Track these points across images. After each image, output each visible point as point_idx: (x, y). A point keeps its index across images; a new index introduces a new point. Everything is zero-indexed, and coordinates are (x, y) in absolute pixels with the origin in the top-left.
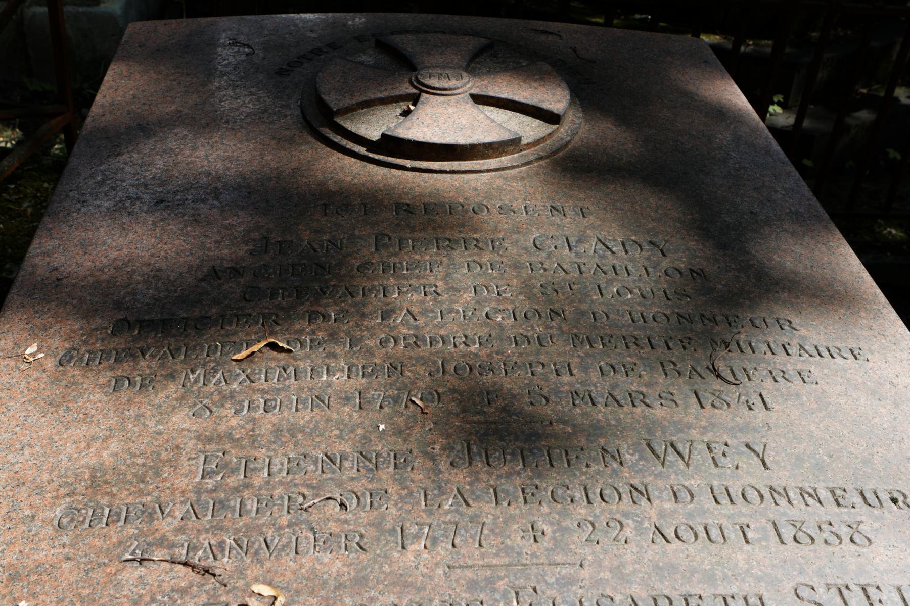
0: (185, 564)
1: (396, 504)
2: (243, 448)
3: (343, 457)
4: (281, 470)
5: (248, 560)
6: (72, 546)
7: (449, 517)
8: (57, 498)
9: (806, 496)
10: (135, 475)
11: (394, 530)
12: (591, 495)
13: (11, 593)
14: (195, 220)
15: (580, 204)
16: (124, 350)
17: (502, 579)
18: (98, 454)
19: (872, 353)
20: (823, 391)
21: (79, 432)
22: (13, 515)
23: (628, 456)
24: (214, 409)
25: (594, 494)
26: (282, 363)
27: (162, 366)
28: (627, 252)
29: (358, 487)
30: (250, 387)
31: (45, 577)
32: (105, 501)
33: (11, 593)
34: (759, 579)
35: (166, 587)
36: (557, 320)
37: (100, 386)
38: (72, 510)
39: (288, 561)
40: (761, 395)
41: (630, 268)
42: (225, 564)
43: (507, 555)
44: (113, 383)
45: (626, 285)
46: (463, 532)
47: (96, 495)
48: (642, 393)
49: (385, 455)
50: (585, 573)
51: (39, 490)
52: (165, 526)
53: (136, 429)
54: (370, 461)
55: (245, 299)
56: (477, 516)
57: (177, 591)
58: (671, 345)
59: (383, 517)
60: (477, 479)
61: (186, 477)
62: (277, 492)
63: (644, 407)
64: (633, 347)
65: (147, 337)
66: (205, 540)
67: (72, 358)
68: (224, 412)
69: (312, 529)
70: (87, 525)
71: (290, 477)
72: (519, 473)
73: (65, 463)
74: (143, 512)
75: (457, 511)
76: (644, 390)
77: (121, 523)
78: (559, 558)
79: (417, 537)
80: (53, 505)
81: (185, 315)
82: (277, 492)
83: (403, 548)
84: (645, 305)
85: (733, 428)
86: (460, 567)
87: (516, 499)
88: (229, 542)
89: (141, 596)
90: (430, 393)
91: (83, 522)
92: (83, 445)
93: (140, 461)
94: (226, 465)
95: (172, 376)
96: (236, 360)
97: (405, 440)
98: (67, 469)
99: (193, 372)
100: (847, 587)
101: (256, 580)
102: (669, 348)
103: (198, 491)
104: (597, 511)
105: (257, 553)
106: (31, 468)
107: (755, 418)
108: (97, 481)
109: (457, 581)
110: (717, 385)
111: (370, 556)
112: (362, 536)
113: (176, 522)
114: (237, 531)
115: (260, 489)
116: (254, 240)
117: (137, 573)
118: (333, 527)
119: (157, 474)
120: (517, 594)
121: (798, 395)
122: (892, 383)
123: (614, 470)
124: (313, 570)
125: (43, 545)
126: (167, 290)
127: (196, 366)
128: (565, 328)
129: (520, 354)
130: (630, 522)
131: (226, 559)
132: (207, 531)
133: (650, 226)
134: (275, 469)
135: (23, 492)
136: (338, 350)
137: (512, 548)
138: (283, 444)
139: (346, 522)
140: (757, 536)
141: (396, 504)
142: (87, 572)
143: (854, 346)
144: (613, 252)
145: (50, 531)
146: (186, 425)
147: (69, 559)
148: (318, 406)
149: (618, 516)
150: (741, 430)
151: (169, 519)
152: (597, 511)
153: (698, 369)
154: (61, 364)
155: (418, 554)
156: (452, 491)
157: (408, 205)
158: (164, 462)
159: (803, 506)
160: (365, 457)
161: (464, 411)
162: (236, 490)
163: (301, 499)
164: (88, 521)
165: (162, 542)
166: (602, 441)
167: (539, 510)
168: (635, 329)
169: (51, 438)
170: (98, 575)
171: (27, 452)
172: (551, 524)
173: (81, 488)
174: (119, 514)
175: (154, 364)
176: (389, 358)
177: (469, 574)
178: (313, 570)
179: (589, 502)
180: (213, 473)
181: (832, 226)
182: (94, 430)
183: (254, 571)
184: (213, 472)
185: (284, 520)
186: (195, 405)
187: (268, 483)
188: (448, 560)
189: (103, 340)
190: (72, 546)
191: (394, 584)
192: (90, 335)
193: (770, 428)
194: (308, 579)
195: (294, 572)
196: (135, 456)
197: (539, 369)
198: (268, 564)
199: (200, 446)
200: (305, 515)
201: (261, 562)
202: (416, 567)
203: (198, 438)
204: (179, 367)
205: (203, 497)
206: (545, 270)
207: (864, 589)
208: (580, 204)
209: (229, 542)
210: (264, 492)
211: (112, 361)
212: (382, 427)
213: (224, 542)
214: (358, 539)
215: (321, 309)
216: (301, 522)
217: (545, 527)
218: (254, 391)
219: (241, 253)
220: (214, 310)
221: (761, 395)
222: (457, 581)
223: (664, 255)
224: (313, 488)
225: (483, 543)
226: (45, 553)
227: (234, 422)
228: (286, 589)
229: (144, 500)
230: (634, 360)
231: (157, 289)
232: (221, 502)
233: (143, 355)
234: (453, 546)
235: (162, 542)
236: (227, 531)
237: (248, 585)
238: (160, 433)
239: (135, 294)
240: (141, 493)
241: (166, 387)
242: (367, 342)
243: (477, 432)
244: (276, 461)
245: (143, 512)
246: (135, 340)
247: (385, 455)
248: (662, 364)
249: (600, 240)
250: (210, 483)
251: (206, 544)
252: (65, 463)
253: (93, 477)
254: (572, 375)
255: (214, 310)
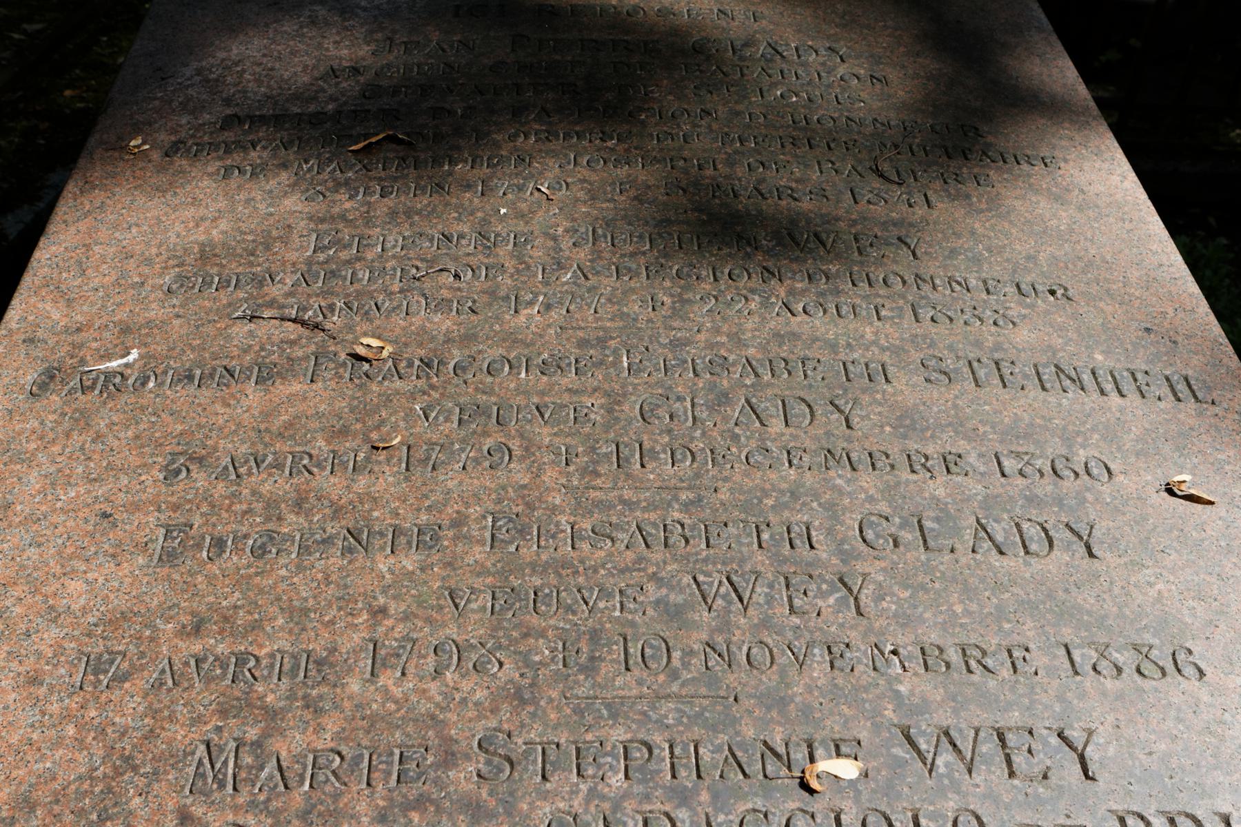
0: (294, 321)
1: (512, 276)
2: (356, 227)
3: (461, 236)
4: (394, 246)
5: (358, 319)
6: (181, 306)
7: (566, 287)
8: (166, 268)
9: (954, 284)
10: (245, 250)
11: (508, 297)
12: (718, 274)
13: (123, 343)
14: (313, 22)
15: (753, 8)
16: (233, 143)
17: (614, 339)
18: (207, 232)
19: (1066, 161)
20: (999, 193)
21: (190, 213)
22: (123, 282)
23: (764, 242)
24: (328, 194)
25: (722, 273)
26: (401, 154)
27: (274, 156)
28: (799, 57)
29: (473, 261)
30: (366, 176)
31: (156, 331)
32: (215, 270)
33: (123, 343)
34: (883, 349)
35: (275, 339)
36: (708, 119)
37: (210, 175)
38: (180, 278)
39: (399, 321)
40: (925, 195)
41: (800, 72)
42: (335, 322)
43: (621, 319)
44: (222, 171)
45: (793, 88)
46: (578, 300)
47: (205, 265)
48: (792, 189)
49: (504, 235)
50: (702, 337)
51: (149, 262)
52: (275, 291)
53: (246, 211)
54: (488, 240)
55: (364, 96)
56: (594, 288)
57: (286, 343)
58: (832, 145)
59: (498, 287)
60: (600, 258)
61: (300, 249)
62: (389, 265)
63: (790, 200)
64: (789, 147)
65: (257, 132)
66: (315, 303)
67: (178, 149)
68: (338, 197)
69: (424, 295)
70: (196, 290)
71: (404, 252)
72: (644, 253)
73: (173, 239)
74: (253, 280)
75: (575, 283)
76: (794, 185)
77: (231, 289)
78: (676, 324)
79: (531, 303)
80: (161, 275)
81: (299, 111)
82: (389, 265)
83: (516, 312)
84: (810, 108)
85: (885, 222)
86: (573, 328)
87: (638, 274)
88: (339, 304)
89: (250, 346)
90: (558, 183)
91: (193, 287)
92: (191, 225)
93: (250, 238)
94: (339, 241)
95: (284, 166)
96: (352, 151)
97: (527, 223)
98: (175, 245)
99: (306, 162)
100: (979, 361)
101: (365, 334)
102: (830, 148)
103: (309, 262)
104: (723, 288)
105: (367, 313)
106: (138, 244)
107: (914, 214)
108: (206, 254)
109: (568, 339)
110: (877, 183)
111: (480, 317)
112: (474, 302)
113: (286, 288)
114: (348, 295)
115: (373, 261)
116: (377, 41)
117: (246, 328)
118: (445, 293)
119: (268, 248)
120: (628, 351)
121: (968, 197)
122: (1082, 191)
123: (747, 253)
124: (423, 328)
125: (154, 306)
126: (280, 88)
127: (311, 156)
128: (715, 126)
129: (661, 150)
130: (756, 297)
131: (335, 318)
132: (318, 295)
133: (832, 32)
134: (388, 245)
135: (132, 264)
136: (462, 143)
137: (628, 315)
138: (398, 224)
139: (459, 289)
140: (890, 314)
141: (512, 276)
142: (197, 327)
143: (1047, 154)
144: (783, 57)
145: (160, 294)
146: (299, 208)
147: (178, 316)
148: (437, 192)
149: (744, 292)
150: (895, 225)
151: (280, 286)
152: (723, 288)
153: (859, 169)
154: (167, 155)
155: (530, 317)
156: (571, 266)
157: (552, 6)
158: (275, 239)
159: (948, 292)
160: (484, 237)
161: (593, 199)
162: (348, 262)
163: (414, 271)
164: (197, 287)
165: (272, 304)
166: (739, 228)
167: (661, 284)
168: (794, 129)
169: (158, 218)
170: (209, 329)
171: (134, 230)
172: (672, 296)
173: (190, 260)
174: (229, 282)
175: (265, 155)
176: (516, 150)
177: (580, 334)
178: (423, 328)
179: (716, 280)
180: (325, 248)
181: (1054, 38)
182: (202, 211)
183: (366, 327)
184: (325, 247)
185: (396, 287)
186: (307, 190)
187: (381, 257)
188: (562, 322)
189: (211, 133)
190: (181, 306)
191: (504, 340)
192: (197, 130)
193: (928, 224)
194: (418, 334)
195: (404, 329)
196: (245, 233)
197: (681, 163)
198: (377, 322)
199: (312, 226)
200: (417, 283)
201: (371, 321)
202: (527, 328)
203: (311, 219)
204: (291, 158)
205: (314, 268)
206: (701, 71)
207: (997, 363)
208: (753, 8)
209: (339, 304)
210: (376, 264)
211: (221, 152)
212: (503, 211)
213: (334, 304)
214: (470, 304)
215: (447, 106)
216: (413, 289)
217: (665, 299)
218: (370, 179)
219: (361, 53)
220: (330, 107)
221: (925, 195)
222: (568, 339)
223: (842, 60)
224: (427, 261)
225: (599, 310)
226: (155, 312)
227: (348, 205)
228: (394, 342)
229: (254, 270)
230: (788, 158)
231: (269, 87)
232: (332, 272)
233: (254, 148)
234: (568, 311)
235: (272, 304)
236: (338, 295)
237: (357, 338)
238: (271, 214)
239: (246, 92)
240: (251, 264)
241: (278, 175)
242: (494, 136)
243: (604, 218)
244: (391, 238)
245: (253, 280)
246: (245, 133)
247: (504, 235)
248: (819, 163)
249: (770, 45)
250: (322, 257)
251: (316, 306)
252: (173, 239)
253: (202, 251)
254: (715, 169)
255: (330, 107)
